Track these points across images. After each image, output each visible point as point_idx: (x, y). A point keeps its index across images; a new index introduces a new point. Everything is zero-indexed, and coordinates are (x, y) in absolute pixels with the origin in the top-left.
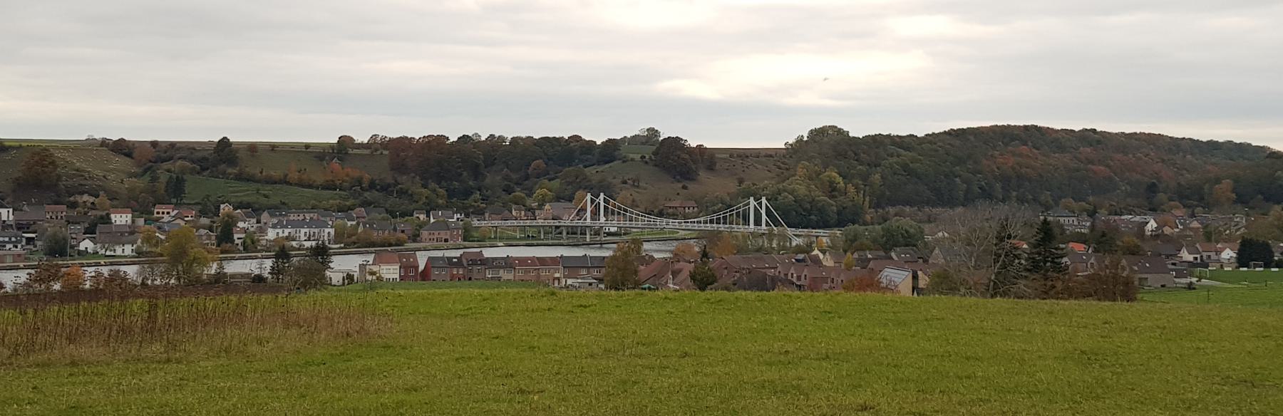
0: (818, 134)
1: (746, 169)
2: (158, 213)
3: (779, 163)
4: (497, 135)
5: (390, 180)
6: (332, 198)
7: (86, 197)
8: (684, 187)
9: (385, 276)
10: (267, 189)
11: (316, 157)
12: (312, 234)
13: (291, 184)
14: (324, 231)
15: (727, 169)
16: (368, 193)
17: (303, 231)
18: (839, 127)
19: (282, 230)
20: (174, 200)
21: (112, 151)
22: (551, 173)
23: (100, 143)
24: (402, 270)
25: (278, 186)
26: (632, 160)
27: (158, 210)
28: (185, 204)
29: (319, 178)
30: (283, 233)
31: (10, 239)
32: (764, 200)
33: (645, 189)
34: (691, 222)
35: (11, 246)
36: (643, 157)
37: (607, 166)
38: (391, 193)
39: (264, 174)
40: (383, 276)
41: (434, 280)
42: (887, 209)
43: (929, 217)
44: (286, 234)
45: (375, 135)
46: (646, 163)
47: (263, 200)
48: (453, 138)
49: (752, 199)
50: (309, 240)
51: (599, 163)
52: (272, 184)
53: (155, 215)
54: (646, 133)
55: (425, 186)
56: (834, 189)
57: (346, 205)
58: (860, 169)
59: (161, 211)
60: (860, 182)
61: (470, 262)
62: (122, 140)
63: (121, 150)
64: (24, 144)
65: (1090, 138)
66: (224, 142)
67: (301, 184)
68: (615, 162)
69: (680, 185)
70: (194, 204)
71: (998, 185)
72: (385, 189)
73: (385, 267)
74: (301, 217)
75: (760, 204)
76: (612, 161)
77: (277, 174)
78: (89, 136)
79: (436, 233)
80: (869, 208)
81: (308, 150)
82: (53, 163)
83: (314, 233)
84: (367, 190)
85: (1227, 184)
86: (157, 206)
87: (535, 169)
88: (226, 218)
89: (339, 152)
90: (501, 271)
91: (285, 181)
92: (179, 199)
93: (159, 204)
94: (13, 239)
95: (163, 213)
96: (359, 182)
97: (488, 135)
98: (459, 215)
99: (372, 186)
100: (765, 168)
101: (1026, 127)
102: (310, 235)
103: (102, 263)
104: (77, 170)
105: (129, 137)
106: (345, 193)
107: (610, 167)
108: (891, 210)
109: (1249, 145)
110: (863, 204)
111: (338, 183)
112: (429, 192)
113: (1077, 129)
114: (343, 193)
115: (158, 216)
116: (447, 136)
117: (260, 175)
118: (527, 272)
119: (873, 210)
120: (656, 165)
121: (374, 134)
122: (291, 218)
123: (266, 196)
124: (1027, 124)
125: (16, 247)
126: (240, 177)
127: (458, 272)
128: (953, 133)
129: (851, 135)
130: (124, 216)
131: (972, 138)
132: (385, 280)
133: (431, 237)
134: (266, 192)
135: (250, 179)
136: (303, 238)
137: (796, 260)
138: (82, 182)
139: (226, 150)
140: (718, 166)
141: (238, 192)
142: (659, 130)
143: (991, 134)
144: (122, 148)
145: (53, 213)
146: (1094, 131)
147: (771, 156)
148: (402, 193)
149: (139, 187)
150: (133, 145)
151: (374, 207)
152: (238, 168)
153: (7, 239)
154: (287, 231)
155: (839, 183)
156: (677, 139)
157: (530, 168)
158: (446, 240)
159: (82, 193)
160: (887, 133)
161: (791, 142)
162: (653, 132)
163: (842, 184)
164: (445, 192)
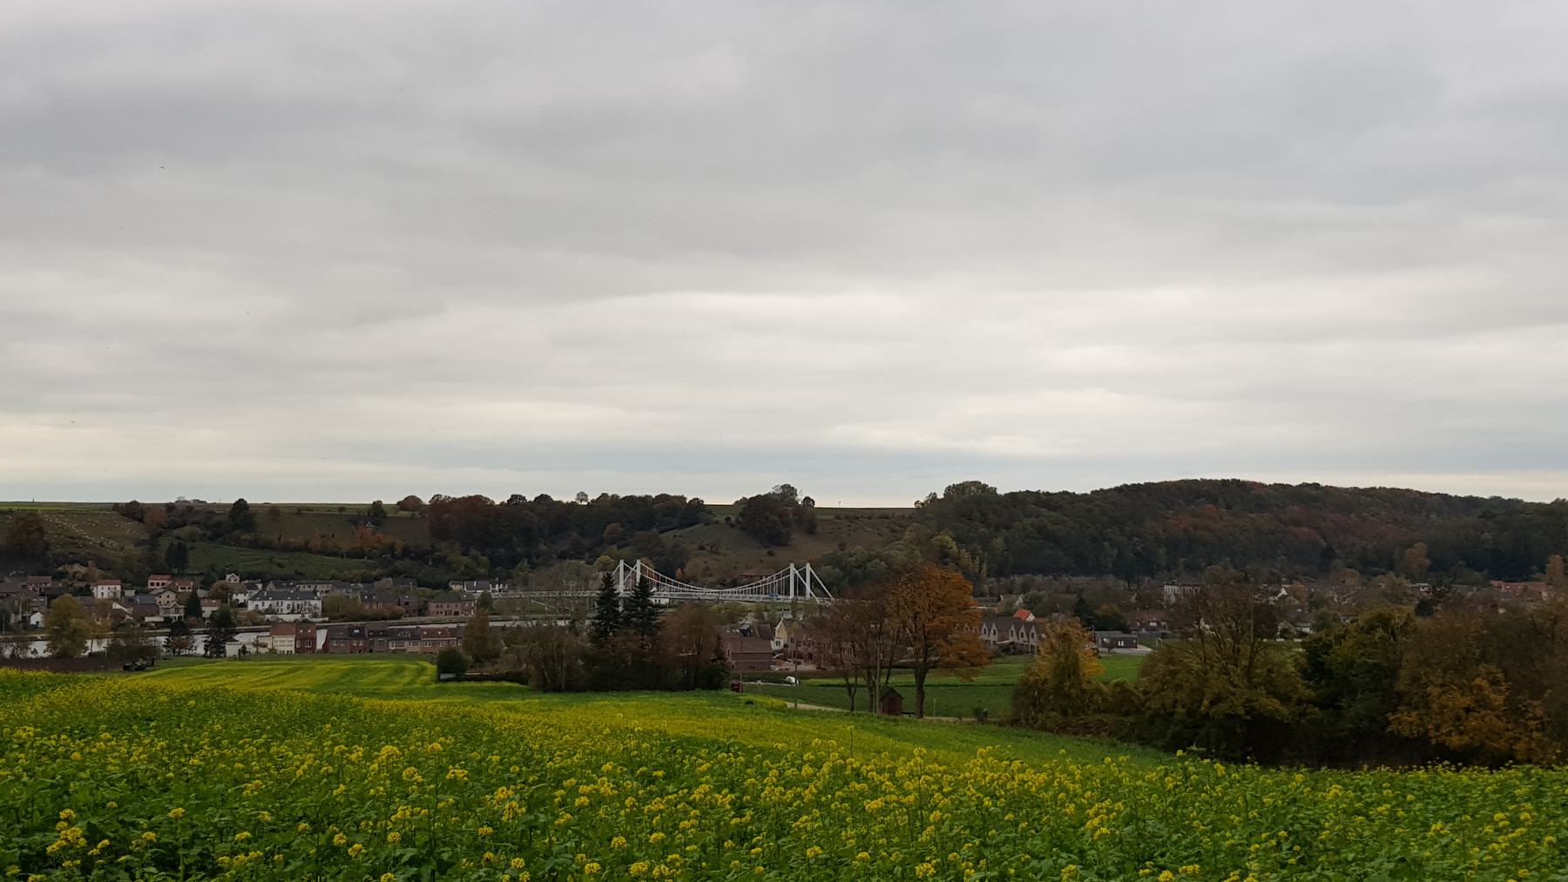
0: (956, 491)
1: (851, 532)
2: (152, 584)
3: (893, 526)
4: (610, 494)
5: (427, 547)
7: (77, 567)
8: (770, 554)
9: (280, 649)
11: (349, 521)
12: (296, 606)
14: (282, 603)
15: (830, 533)
16: (400, 562)
17: (286, 603)
18: (983, 483)
21: (122, 514)
22: (627, 537)
23: (229, 509)
24: (298, 642)
25: (297, 554)
26: (717, 522)
27: (153, 581)
29: (345, 546)
30: (263, 605)
32: (808, 567)
33: (725, 556)
36: (728, 519)
37: (687, 530)
39: (282, 540)
40: (276, 648)
41: (333, 653)
42: (1012, 578)
43: (1068, 587)
44: (266, 606)
46: (732, 526)
47: (277, 570)
48: (530, 498)
51: (682, 526)
52: (291, 551)
53: (150, 587)
55: (465, 554)
56: (946, 555)
58: (983, 532)
60: (979, 547)
61: (371, 634)
62: (134, 503)
63: (134, 514)
64: (15, 508)
65: (1311, 495)
66: (241, 504)
67: (324, 552)
68: (697, 526)
69: (765, 551)
70: (197, 575)
71: (1162, 551)
72: (421, 556)
73: (278, 639)
74: (312, 589)
75: (803, 574)
76: (693, 524)
79: (445, 605)
80: (988, 576)
81: (343, 513)
82: (40, 529)
83: (298, 605)
84: (399, 559)
85: (1420, 548)
86: (152, 577)
87: (611, 533)
88: (220, 590)
89: (376, 515)
90: (407, 643)
91: (306, 548)
95: (158, 584)
96: (391, 548)
98: (501, 586)
99: (406, 552)
100: (876, 532)
101: (1224, 482)
104: (71, 538)
105: (145, 498)
106: (374, 562)
108: (1017, 578)
109: (1519, 502)
110: (980, 571)
111: (367, 549)
112: (470, 560)
113: (1294, 484)
114: (370, 561)
116: (523, 495)
118: (435, 643)
119: (993, 579)
121: (436, 494)
122: (301, 589)
123: (280, 565)
124: (1226, 478)
126: (255, 545)
127: (358, 643)
128: (1125, 489)
129: (998, 492)
131: (1144, 495)
133: (439, 610)
135: (267, 546)
136: (285, 611)
137: (741, 630)
139: (242, 514)
140: (819, 529)
142: (796, 487)
143: (1418, 495)
145: (36, 584)
146: (1316, 486)
147: (887, 518)
148: (440, 561)
150: (148, 508)
151: (405, 577)
152: (253, 534)
154: (267, 603)
155: (951, 548)
156: (478, 498)
158: (457, 613)
159: (72, 563)
160: (1553, 500)
161: (922, 501)
162: (789, 491)
163: (955, 549)
164: (488, 561)
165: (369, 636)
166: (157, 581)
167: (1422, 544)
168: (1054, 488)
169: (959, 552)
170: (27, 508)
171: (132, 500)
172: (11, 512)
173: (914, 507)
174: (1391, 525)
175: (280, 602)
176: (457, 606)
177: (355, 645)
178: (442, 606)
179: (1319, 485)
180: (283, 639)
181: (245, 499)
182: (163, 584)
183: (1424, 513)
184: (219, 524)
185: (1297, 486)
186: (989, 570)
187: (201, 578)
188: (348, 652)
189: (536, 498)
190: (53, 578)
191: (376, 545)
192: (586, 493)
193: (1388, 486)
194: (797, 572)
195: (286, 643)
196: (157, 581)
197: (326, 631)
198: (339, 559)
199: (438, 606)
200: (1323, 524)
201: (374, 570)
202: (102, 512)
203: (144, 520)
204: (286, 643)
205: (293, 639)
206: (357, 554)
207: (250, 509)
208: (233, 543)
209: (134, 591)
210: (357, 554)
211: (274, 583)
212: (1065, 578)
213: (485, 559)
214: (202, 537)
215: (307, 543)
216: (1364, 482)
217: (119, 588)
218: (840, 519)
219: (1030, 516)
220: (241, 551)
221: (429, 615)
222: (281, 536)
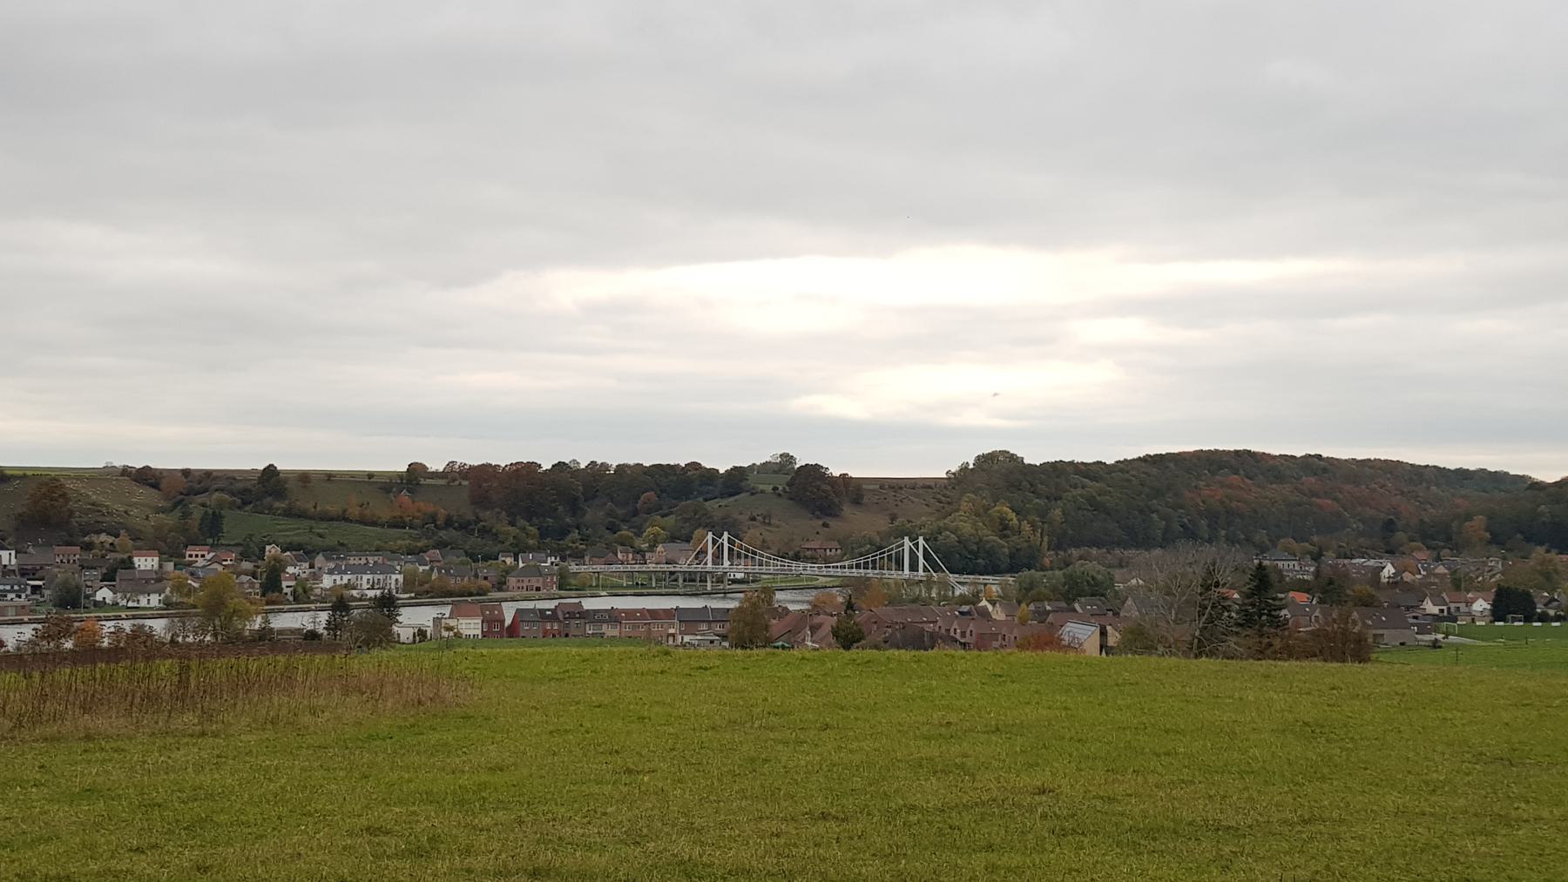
0: (986, 461)
1: (899, 503)
2: (191, 556)
3: (939, 496)
4: (599, 462)
6: (401, 538)
7: (103, 537)
8: (825, 525)
9: (465, 632)
10: (321, 527)
11: (380, 488)
13: (351, 521)
16: (444, 532)
17: (365, 577)
19: (339, 576)
20: (210, 541)
21: (135, 481)
24: (484, 625)
25: (335, 524)
26: (762, 492)
27: (192, 553)
28: (223, 545)
29: (385, 514)
30: (341, 579)
31: (12, 587)
32: (921, 540)
33: (778, 527)
34: (833, 567)
35: (13, 595)
36: (775, 489)
37: (732, 499)
38: (471, 532)
39: (318, 508)
40: (461, 631)
41: (523, 637)
45: (453, 462)
46: (779, 495)
48: (546, 466)
49: (906, 539)
50: (373, 589)
51: (722, 496)
53: (187, 558)
54: (779, 459)
55: (512, 524)
56: (1006, 527)
57: (416, 546)
58: (1037, 503)
59: (194, 553)
60: (1037, 519)
61: (567, 616)
64: (29, 473)
65: (1314, 465)
66: (270, 471)
67: (363, 521)
68: (742, 495)
69: (821, 522)
70: (234, 545)
72: (464, 527)
74: (363, 561)
75: (917, 545)
77: (334, 509)
78: (107, 463)
79: (526, 580)
80: (1048, 549)
82: (63, 495)
83: (379, 580)
84: (442, 529)
85: (1479, 521)
87: (645, 503)
88: (273, 562)
89: (409, 482)
90: (605, 626)
91: (343, 518)
92: (216, 539)
93: (192, 545)
94: (16, 588)
96: (433, 518)
97: (589, 462)
98: (553, 558)
99: (449, 523)
101: (1237, 452)
102: (373, 582)
103: (124, 616)
104: (93, 505)
105: (157, 464)
107: (736, 501)
108: (1074, 552)
110: (1041, 544)
111: (407, 519)
112: (518, 531)
113: (1298, 455)
114: (411, 531)
115: (190, 559)
117: (313, 510)
118: (635, 627)
119: (1052, 552)
120: (791, 499)
122: (351, 562)
123: (321, 536)
125: (20, 597)
126: (289, 513)
127: (552, 627)
128: (1149, 459)
130: (149, 559)
131: (1172, 465)
132: (464, 637)
133: (520, 585)
134: (321, 531)
135: (302, 515)
138: (100, 519)
140: (865, 500)
141: (287, 530)
142: (795, 456)
144: (146, 477)
145: (63, 555)
146: (1319, 457)
147: (930, 487)
148: (485, 532)
149: (168, 524)
152: (286, 502)
153: (8, 588)
154: (346, 578)
155: (1012, 520)
156: (817, 467)
157: (640, 502)
158: (538, 589)
159: (99, 532)
162: (787, 459)
163: (1015, 521)
164: (537, 531)
165: (565, 618)
166: (196, 553)
167: (1481, 517)
168: (1089, 459)
169: (1020, 525)
170: (53, 474)
171: (144, 465)
172: (25, 476)
173: (945, 476)
174: (1399, 497)
175: (359, 576)
176: (153, 560)
177: (549, 628)
178: (523, 581)
179: (1321, 456)
180: (469, 621)
181: (275, 465)
182: (203, 556)
183: (1424, 485)
184: (246, 491)
185: (1302, 457)
186: (1049, 543)
187: (240, 549)
188: (541, 635)
189: (553, 466)
190: (82, 548)
191: (418, 514)
192: (578, 461)
193: (1383, 458)
194: (911, 544)
195: (472, 626)
196: (196, 553)
197: (451, 606)
198: (378, 529)
199: (519, 581)
200: (1341, 496)
201: (419, 542)
202: (114, 478)
203: (162, 486)
204: (472, 626)
205: (480, 621)
206: (397, 524)
207: (281, 475)
208: (266, 512)
209: (172, 563)
210: (397, 524)
211: (324, 555)
212: (1117, 551)
213: (533, 530)
214: (232, 506)
215: (345, 511)
216: (1450, 459)
217: (156, 559)
218: (884, 489)
219: (1075, 487)
220: (275, 520)
221: (508, 591)
222: (316, 504)
